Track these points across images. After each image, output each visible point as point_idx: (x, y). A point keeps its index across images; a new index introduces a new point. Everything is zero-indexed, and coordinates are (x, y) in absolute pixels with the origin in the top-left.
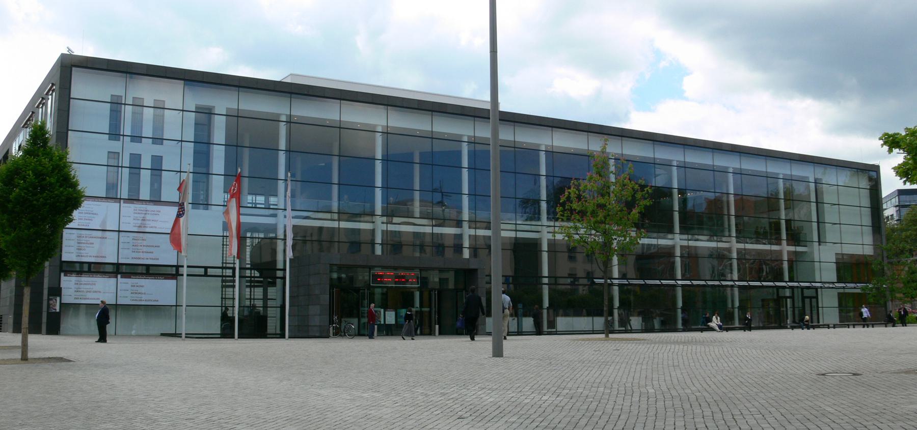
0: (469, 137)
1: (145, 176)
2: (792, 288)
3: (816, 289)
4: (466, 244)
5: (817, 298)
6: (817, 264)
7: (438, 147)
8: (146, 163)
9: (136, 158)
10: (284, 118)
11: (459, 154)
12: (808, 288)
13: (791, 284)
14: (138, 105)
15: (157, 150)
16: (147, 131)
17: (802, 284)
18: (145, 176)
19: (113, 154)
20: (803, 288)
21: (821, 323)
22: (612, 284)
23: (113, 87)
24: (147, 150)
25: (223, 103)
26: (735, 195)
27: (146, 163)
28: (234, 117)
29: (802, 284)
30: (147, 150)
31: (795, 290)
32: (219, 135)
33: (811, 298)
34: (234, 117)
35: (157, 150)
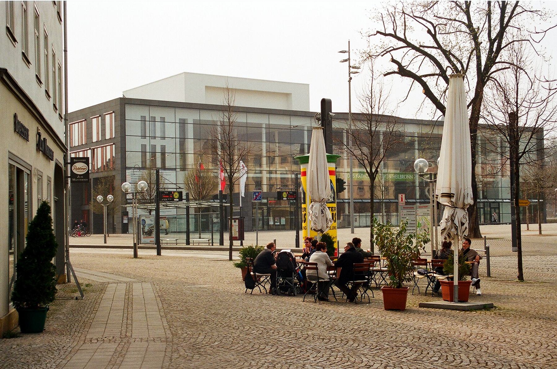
0: (266, 124)
1: (158, 156)
2: (484, 202)
3: (499, 203)
4: (265, 182)
5: (499, 208)
6: (500, 189)
7: (250, 131)
8: (158, 150)
9: (154, 147)
10: (264, 126)
11: (261, 134)
12: (494, 202)
13: (484, 200)
14: (153, 120)
15: (163, 142)
16: (158, 134)
17: (490, 200)
18: (158, 156)
19: (144, 146)
20: (490, 203)
21: (501, 222)
22: (344, 202)
23: (144, 112)
24: (158, 143)
25: (191, 117)
26: (415, 149)
27: (158, 150)
28: (196, 124)
29: (490, 200)
30: (158, 143)
31: (486, 204)
32: (190, 133)
33: (495, 208)
34: (196, 124)
35: (163, 142)
